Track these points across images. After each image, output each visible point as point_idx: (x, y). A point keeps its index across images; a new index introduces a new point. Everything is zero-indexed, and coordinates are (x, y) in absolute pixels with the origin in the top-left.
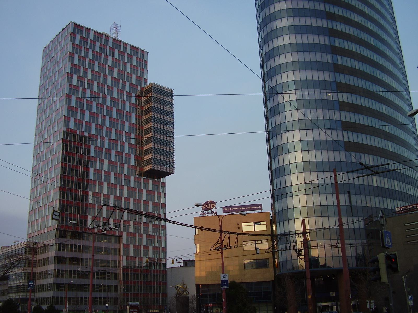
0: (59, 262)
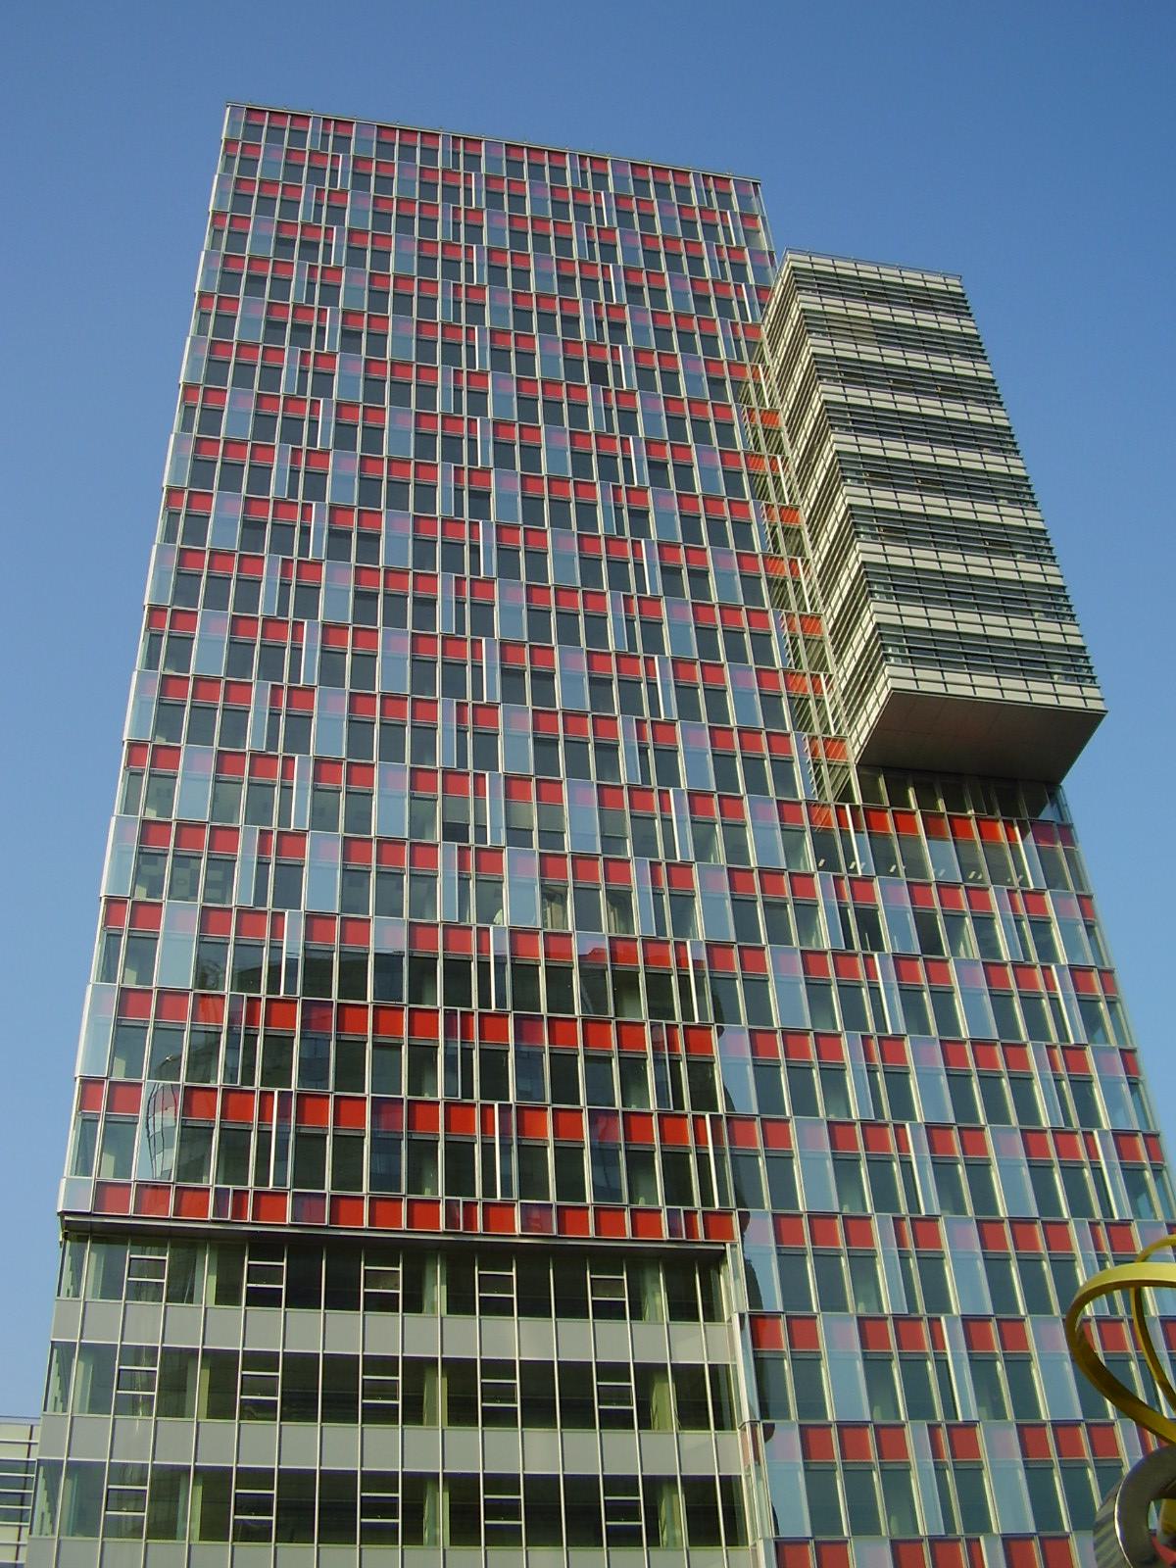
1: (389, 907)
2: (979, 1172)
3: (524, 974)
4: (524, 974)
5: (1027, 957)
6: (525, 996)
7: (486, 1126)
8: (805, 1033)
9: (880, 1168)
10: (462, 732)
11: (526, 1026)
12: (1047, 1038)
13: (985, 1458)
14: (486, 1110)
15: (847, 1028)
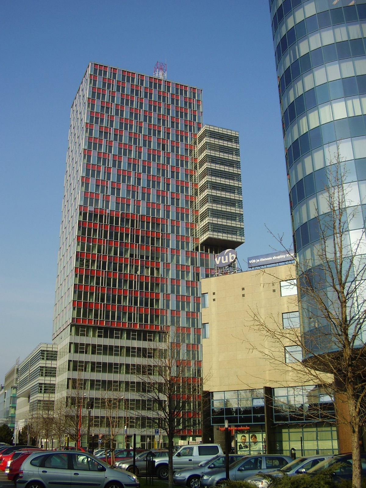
0: (75, 369)
1: (91, 205)
2: (178, 228)
3: (112, 218)
4: (112, 218)
5: (191, 97)
6: (111, 222)
7: (103, 274)
8: (156, 150)
9: (163, 197)
10: (110, 96)
11: (109, 289)
12: (191, 108)
13: (170, 299)
14: (103, 271)
15: (162, 176)
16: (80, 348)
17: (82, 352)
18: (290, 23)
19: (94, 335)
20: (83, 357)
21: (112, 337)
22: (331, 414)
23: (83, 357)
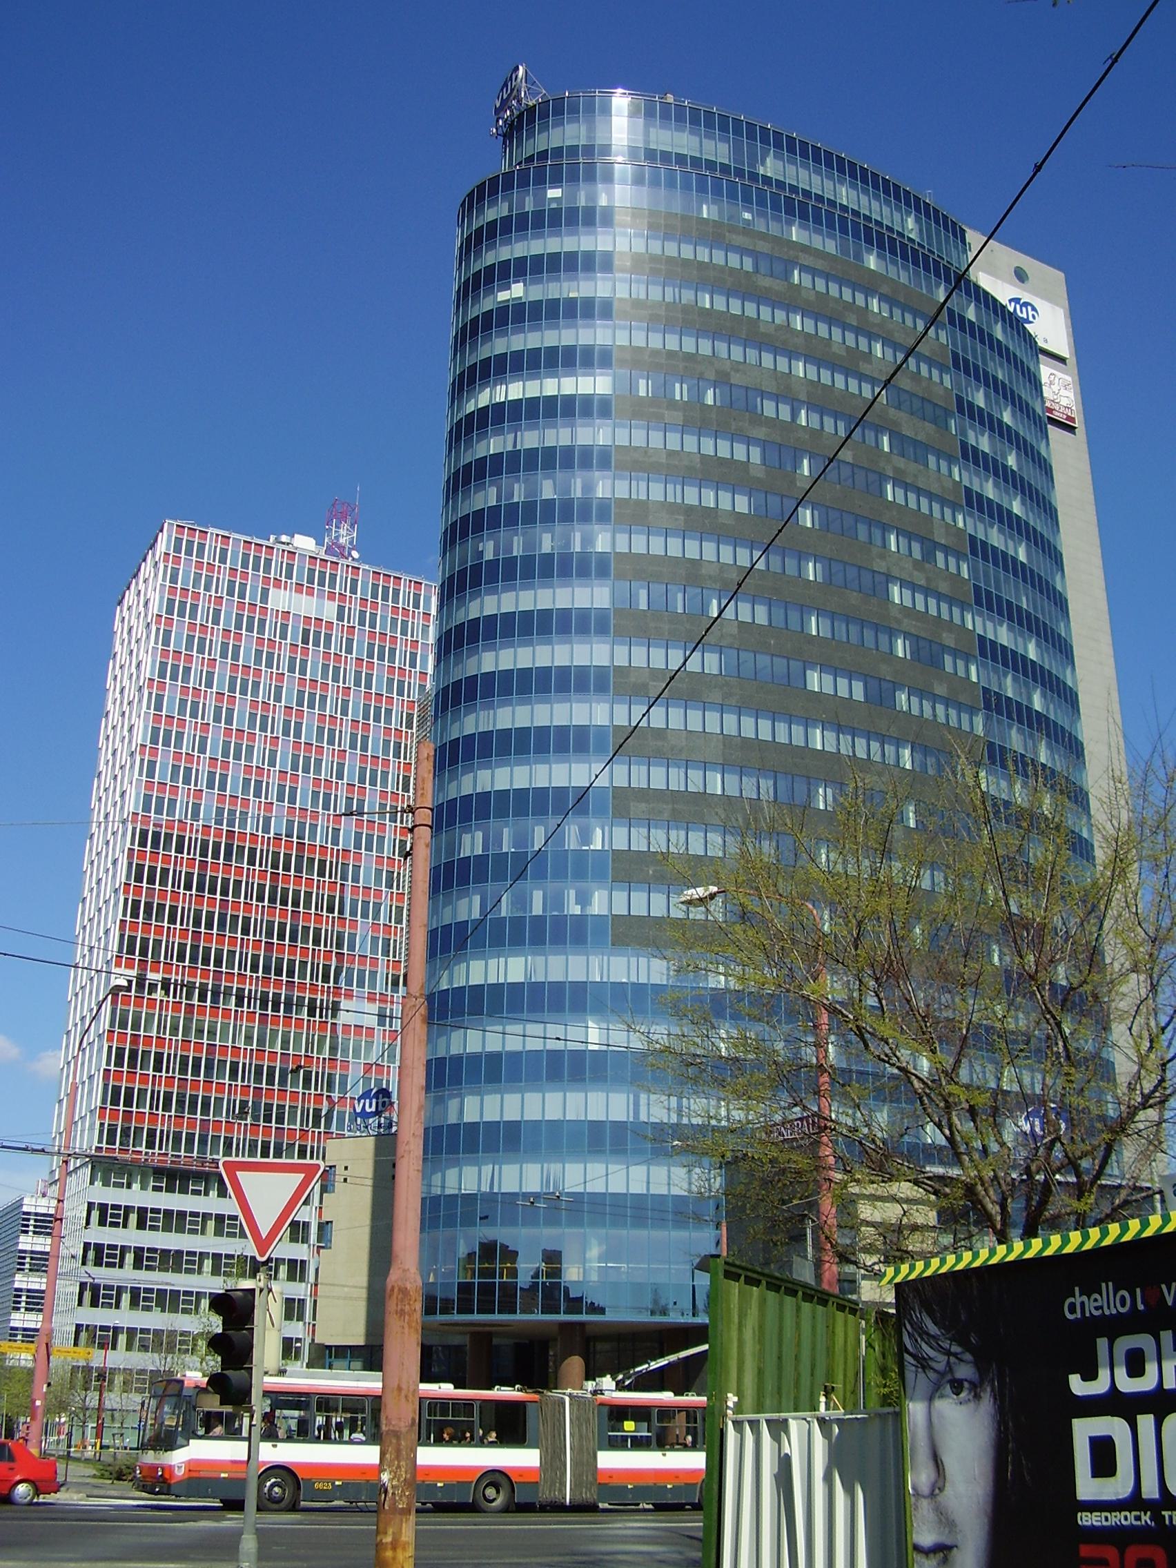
16: (112, 1216)
17: (115, 1225)
18: (484, 398)
19: (143, 1188)
20: (104, 1275)
21: (184, 1190)
22: (558, 436)
23: (104, 1275)
